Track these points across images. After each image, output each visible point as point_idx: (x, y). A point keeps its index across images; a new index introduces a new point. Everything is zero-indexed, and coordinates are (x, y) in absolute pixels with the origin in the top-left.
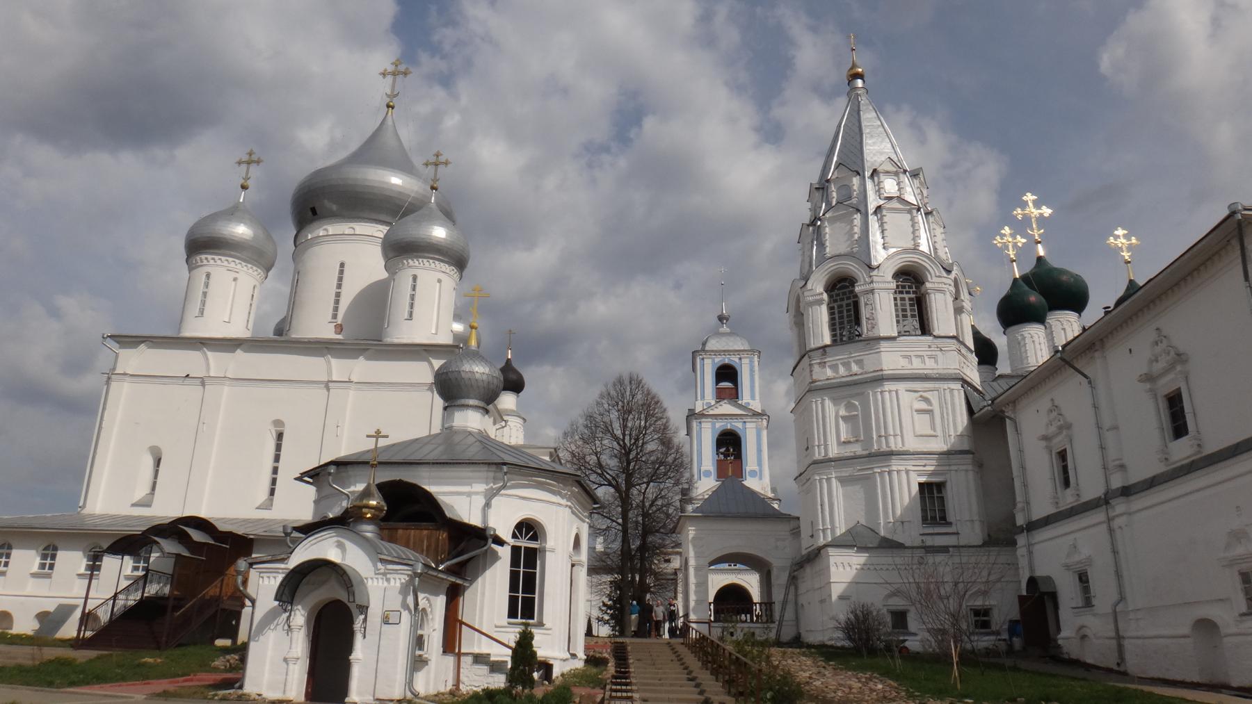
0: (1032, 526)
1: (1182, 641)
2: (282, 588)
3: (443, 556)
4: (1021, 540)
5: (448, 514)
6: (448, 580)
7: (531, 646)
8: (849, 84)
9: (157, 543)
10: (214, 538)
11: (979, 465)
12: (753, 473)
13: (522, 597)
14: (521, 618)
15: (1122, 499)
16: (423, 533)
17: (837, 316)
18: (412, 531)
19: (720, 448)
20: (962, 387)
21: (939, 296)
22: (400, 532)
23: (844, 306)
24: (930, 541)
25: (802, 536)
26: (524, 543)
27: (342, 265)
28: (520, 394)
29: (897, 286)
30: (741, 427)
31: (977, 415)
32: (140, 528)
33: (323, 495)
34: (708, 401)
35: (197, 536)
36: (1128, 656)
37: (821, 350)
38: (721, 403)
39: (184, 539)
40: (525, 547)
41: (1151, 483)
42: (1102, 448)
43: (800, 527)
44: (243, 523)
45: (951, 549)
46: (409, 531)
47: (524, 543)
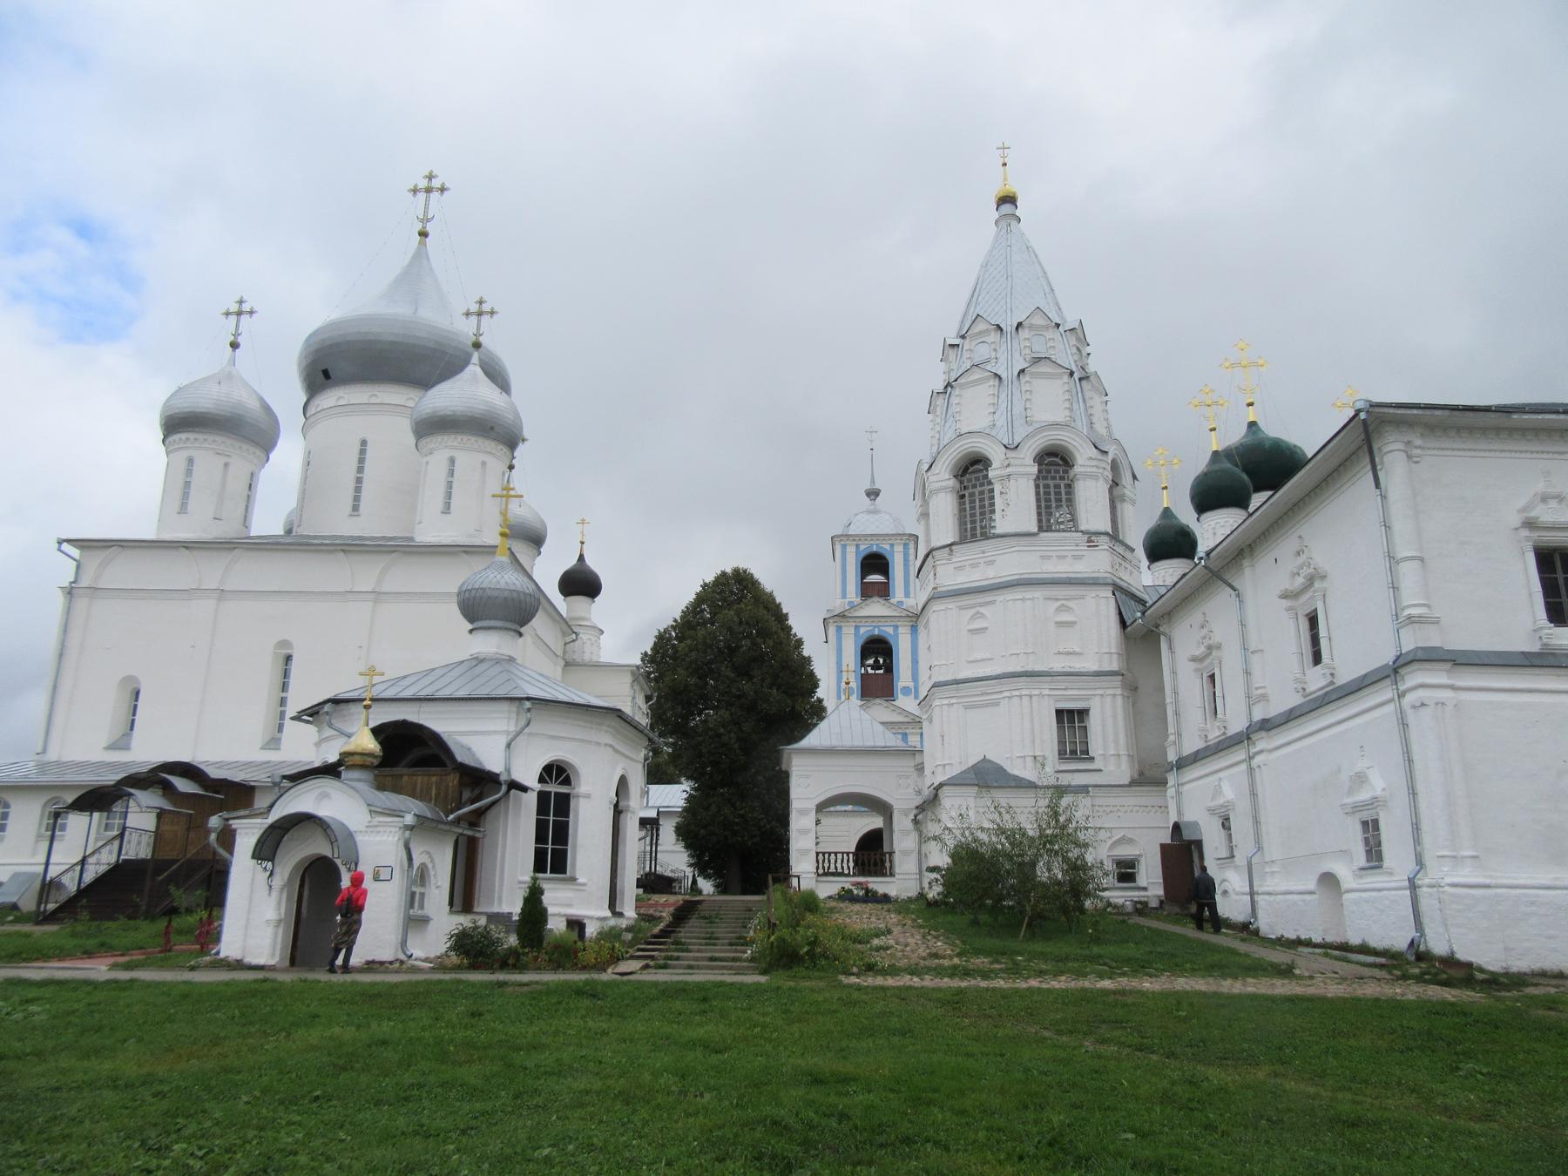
0: (1182, 764)
1: (1307, 897)
2: (259, 847)
3: (453, 805)
4: (1172, 779)
5: (461, 757)
6: (465, 835)
7: (541, 902)
8: (997, 209)
9: (130, 795)
10: (205, 788)
11: (1132, 689)
12: (906, 691)
13: (548, 844)
14: (550, 873)
15: (1263, 734)
16: (428, 778)
17: (987, 502)
18: (419, 778)
19: (867, 660)
20: (1114, 594)
21: (1090, 483)
22: (405, 778)
23: (977, 494)
24: (1065, 780)
25: (926, 773)
26: (553, 788)
27: (364, 443)
28: (596, 599)
29: (1040, 471)
30: (892, 632)
31: (1129, 629)
32: (111, 778)
33: (324, 736)
34: (851, 600)
35: (182, 785)
36: (1261, 914)
37: (948, 549)
38: (868, 602)
39: (168, 789)
40: (556, 793)
41: (1291, 717)
42: (1247, 673)
43: (923, 763)
44: (446, 670)
45: (1090, 789)
46: (414, 778)
47: (553, 788)
